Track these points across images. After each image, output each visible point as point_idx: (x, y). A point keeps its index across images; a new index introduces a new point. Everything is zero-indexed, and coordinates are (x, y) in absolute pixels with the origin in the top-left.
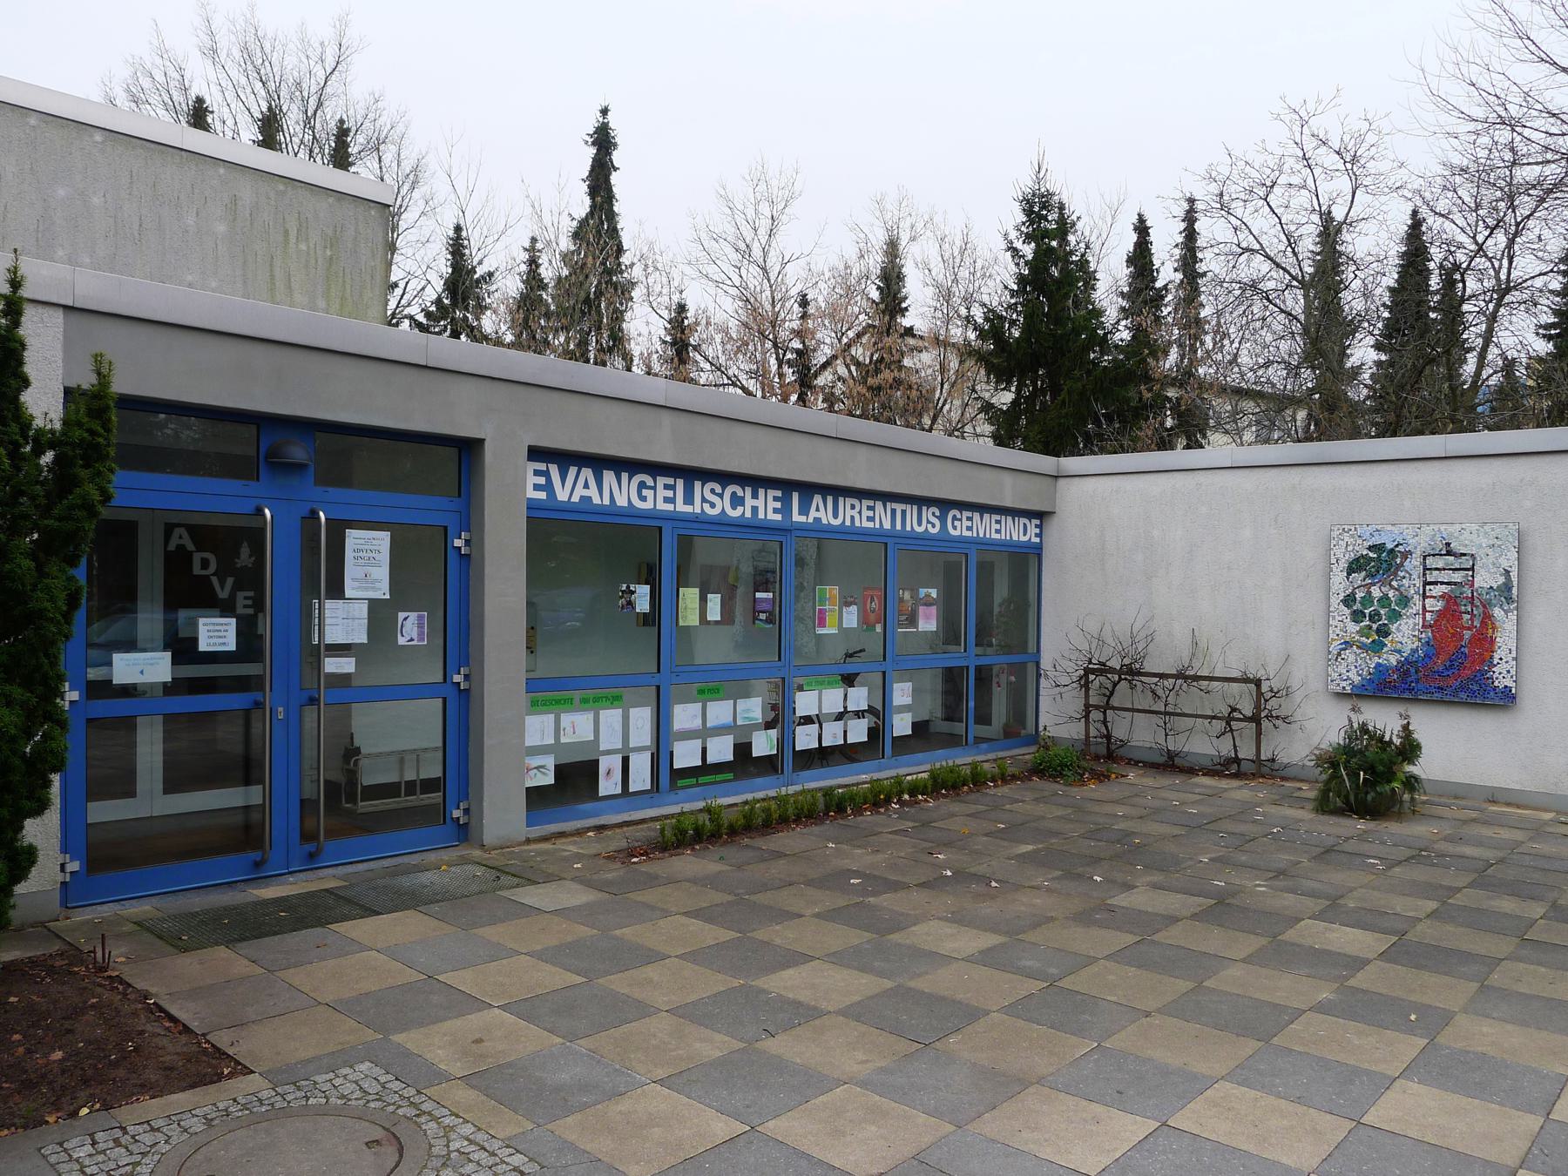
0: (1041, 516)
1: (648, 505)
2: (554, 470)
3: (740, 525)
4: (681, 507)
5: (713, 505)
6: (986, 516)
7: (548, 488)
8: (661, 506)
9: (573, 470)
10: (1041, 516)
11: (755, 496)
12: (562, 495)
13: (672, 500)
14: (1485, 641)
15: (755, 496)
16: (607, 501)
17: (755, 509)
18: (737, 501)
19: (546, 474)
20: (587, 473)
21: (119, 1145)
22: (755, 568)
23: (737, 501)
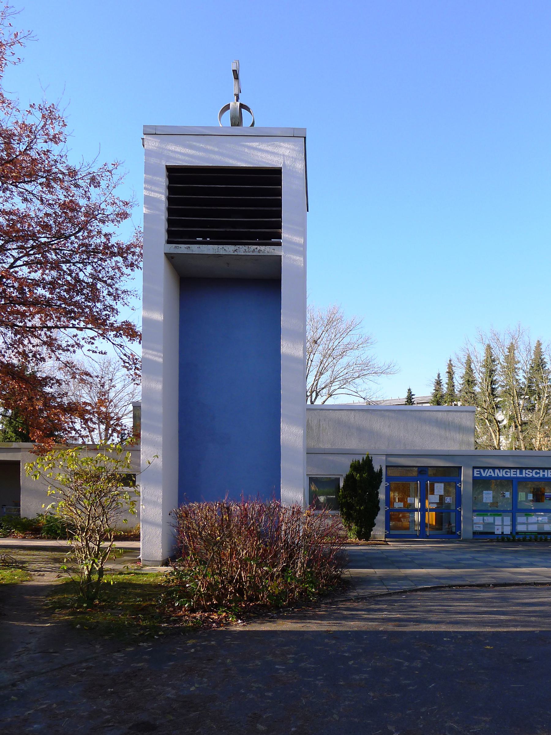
0: (299, 136)
1: (509, 475)
2: (482, 470)
3: (539, 478)
4: (518, 475)
5: (529, 475)
6: (501, 470)
7: (480, 474)
8: (512, 475)
9: (487, 470)
10: (299, 136)
11: (544, 472)
12: (484, 475)
13: (516, 474)
14: (371, 461)
15: (544, 472)
16: (496, 475)
17: (544, 475)
18: (521, 473)
19: (480, 471)
20: (491, 470)
21: (91, 494)
22: (134, 485)
23: (536, 473)
